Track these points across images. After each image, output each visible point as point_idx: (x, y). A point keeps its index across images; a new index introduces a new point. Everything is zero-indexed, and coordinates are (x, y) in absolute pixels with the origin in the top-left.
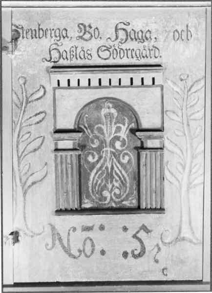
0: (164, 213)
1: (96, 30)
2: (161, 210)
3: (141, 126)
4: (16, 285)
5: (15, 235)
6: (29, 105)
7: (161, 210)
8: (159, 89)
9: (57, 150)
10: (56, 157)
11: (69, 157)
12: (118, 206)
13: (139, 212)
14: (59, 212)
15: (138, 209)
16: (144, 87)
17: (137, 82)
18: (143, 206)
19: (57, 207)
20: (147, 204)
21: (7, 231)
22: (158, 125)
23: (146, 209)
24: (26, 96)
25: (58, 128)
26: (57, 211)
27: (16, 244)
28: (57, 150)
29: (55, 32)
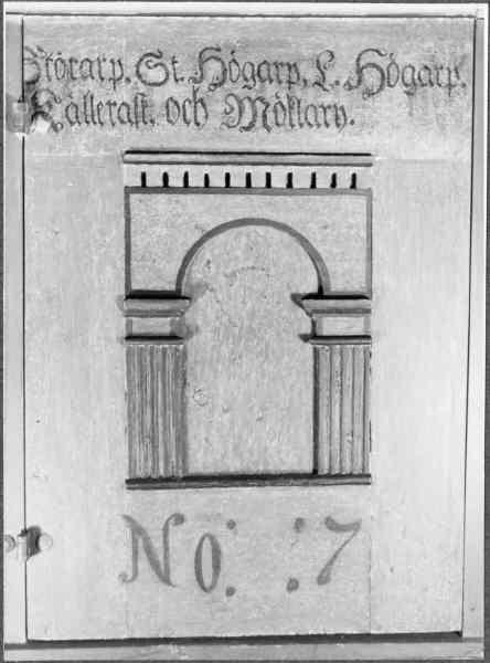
0: (369, 484)
1: (233, 64)
2: (363, 478)
3: (328, 289)
4: (34, 644)
5: (33, 539)
6: (453, 91)
7: (363, 478)
8: (363, 200)
9: (130, 337)
10: (129, 353)
11: (158, 358)
12: (161, 346)
13: (316, 481)
14: (135, 483)
15: (314, 477)
16: (337, 193)
17: (324, 183)
18: (324, 469)
19: (130, 472)
20: (341, 469)
21: (12, 528)
22: (356, 286)
23: (329, 476)
24: (100, 72)
25: (135, 286)
26: (128, 482)
27: (35, 558)
28: (130, 337)
29: (119, 110)
